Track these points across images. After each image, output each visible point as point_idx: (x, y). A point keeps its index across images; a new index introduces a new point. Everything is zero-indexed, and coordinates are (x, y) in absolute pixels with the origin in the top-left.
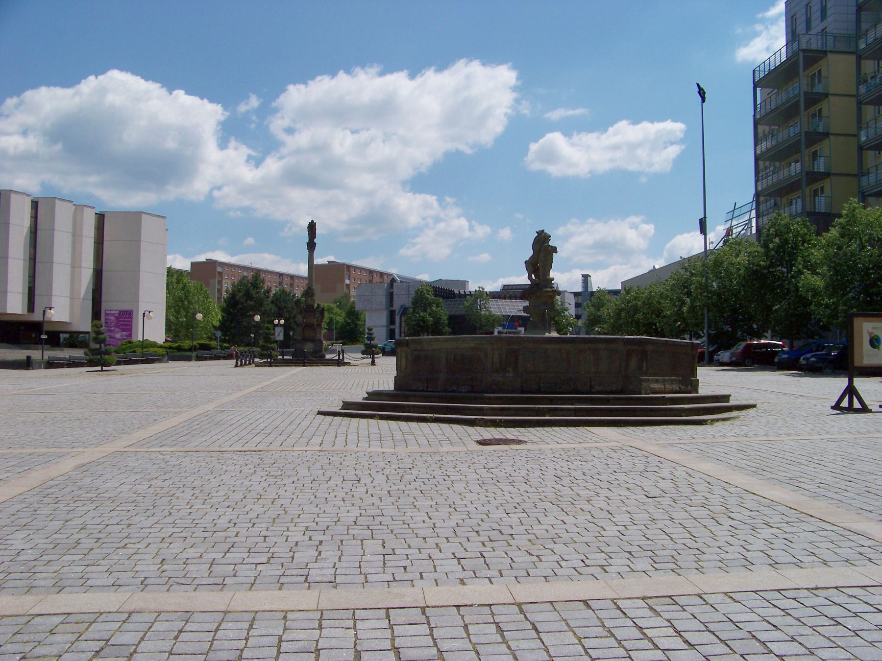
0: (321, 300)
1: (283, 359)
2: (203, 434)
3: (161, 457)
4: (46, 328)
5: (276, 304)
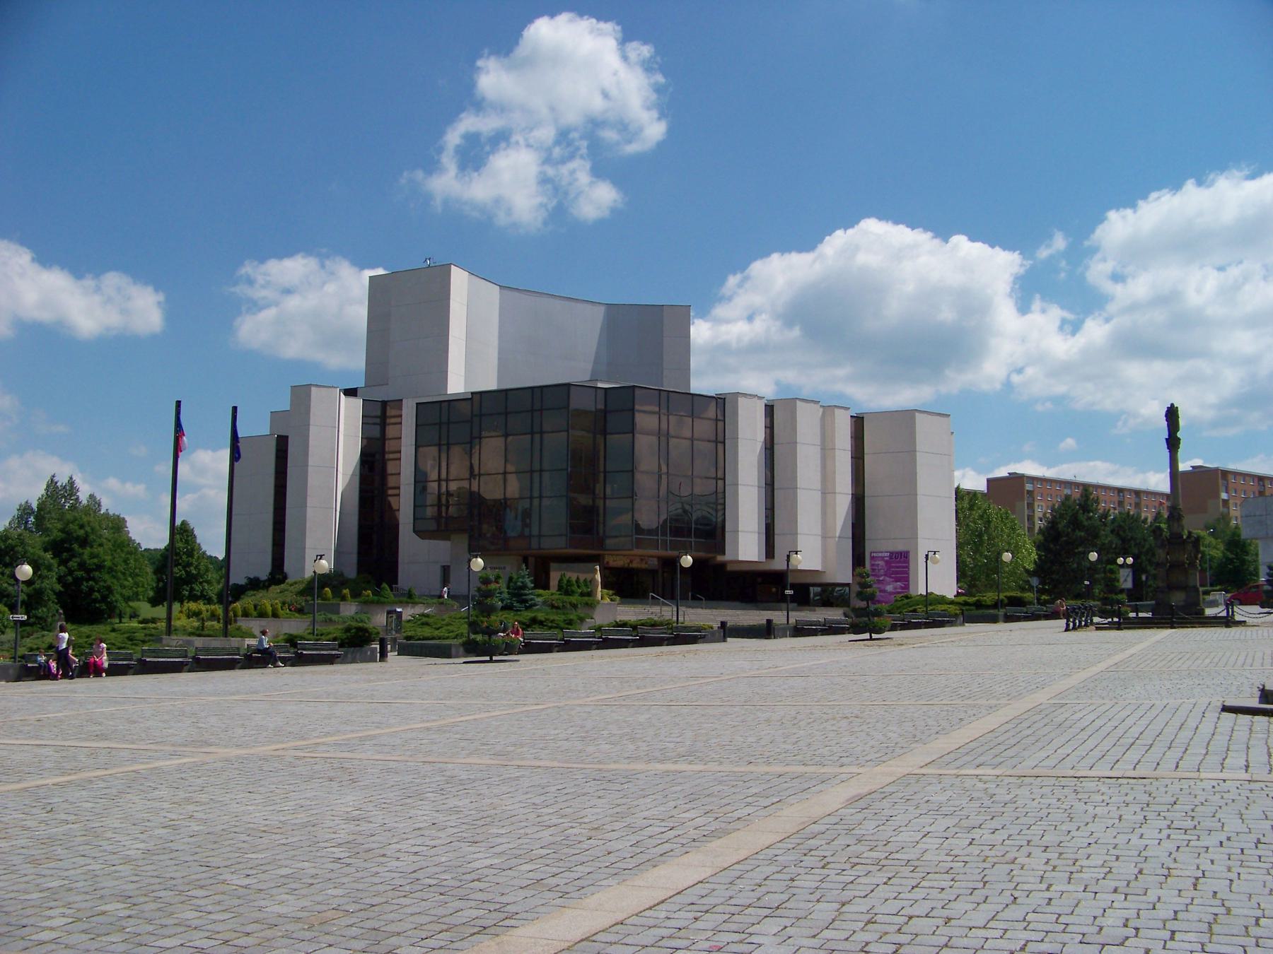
0: (1192, 525)
1: (1137, 618)
2: (1040, 744)
3: (980, 785)
4: (791, 580)
5: (1118, 534)
